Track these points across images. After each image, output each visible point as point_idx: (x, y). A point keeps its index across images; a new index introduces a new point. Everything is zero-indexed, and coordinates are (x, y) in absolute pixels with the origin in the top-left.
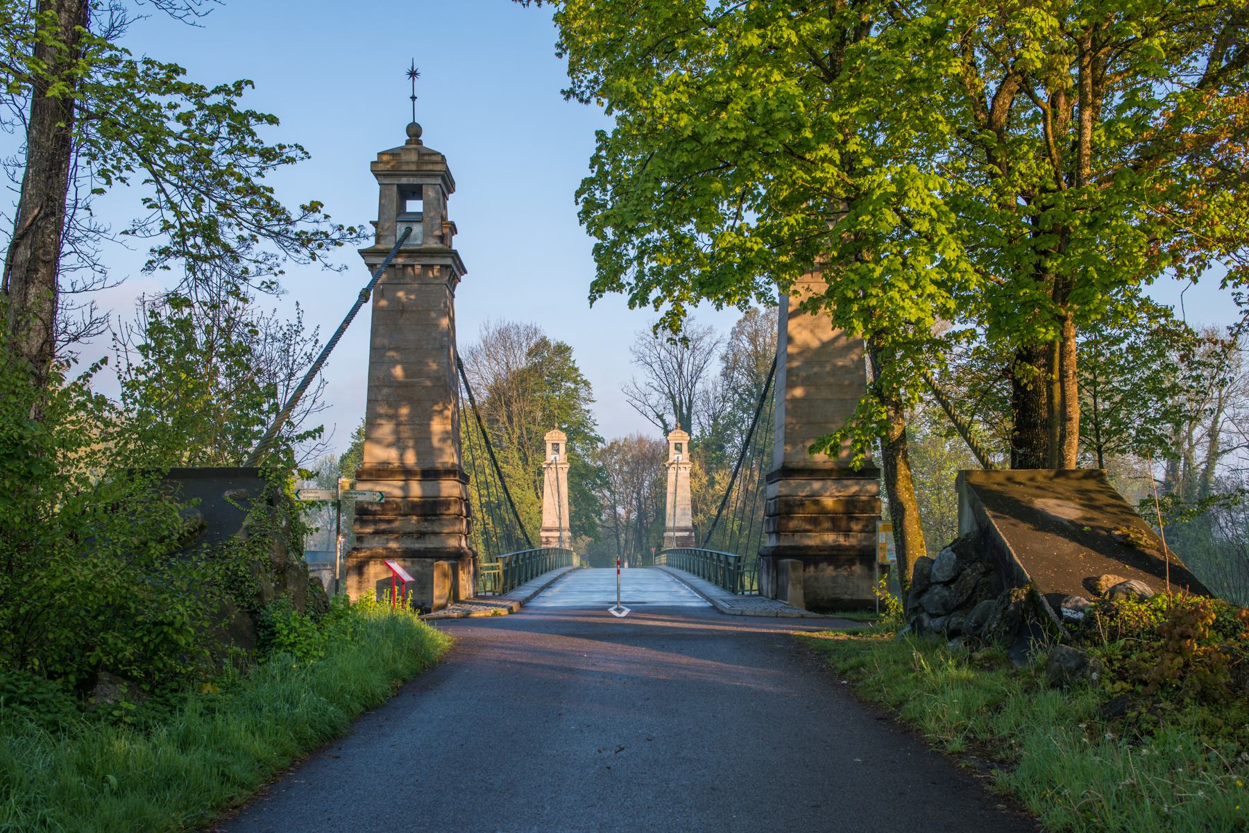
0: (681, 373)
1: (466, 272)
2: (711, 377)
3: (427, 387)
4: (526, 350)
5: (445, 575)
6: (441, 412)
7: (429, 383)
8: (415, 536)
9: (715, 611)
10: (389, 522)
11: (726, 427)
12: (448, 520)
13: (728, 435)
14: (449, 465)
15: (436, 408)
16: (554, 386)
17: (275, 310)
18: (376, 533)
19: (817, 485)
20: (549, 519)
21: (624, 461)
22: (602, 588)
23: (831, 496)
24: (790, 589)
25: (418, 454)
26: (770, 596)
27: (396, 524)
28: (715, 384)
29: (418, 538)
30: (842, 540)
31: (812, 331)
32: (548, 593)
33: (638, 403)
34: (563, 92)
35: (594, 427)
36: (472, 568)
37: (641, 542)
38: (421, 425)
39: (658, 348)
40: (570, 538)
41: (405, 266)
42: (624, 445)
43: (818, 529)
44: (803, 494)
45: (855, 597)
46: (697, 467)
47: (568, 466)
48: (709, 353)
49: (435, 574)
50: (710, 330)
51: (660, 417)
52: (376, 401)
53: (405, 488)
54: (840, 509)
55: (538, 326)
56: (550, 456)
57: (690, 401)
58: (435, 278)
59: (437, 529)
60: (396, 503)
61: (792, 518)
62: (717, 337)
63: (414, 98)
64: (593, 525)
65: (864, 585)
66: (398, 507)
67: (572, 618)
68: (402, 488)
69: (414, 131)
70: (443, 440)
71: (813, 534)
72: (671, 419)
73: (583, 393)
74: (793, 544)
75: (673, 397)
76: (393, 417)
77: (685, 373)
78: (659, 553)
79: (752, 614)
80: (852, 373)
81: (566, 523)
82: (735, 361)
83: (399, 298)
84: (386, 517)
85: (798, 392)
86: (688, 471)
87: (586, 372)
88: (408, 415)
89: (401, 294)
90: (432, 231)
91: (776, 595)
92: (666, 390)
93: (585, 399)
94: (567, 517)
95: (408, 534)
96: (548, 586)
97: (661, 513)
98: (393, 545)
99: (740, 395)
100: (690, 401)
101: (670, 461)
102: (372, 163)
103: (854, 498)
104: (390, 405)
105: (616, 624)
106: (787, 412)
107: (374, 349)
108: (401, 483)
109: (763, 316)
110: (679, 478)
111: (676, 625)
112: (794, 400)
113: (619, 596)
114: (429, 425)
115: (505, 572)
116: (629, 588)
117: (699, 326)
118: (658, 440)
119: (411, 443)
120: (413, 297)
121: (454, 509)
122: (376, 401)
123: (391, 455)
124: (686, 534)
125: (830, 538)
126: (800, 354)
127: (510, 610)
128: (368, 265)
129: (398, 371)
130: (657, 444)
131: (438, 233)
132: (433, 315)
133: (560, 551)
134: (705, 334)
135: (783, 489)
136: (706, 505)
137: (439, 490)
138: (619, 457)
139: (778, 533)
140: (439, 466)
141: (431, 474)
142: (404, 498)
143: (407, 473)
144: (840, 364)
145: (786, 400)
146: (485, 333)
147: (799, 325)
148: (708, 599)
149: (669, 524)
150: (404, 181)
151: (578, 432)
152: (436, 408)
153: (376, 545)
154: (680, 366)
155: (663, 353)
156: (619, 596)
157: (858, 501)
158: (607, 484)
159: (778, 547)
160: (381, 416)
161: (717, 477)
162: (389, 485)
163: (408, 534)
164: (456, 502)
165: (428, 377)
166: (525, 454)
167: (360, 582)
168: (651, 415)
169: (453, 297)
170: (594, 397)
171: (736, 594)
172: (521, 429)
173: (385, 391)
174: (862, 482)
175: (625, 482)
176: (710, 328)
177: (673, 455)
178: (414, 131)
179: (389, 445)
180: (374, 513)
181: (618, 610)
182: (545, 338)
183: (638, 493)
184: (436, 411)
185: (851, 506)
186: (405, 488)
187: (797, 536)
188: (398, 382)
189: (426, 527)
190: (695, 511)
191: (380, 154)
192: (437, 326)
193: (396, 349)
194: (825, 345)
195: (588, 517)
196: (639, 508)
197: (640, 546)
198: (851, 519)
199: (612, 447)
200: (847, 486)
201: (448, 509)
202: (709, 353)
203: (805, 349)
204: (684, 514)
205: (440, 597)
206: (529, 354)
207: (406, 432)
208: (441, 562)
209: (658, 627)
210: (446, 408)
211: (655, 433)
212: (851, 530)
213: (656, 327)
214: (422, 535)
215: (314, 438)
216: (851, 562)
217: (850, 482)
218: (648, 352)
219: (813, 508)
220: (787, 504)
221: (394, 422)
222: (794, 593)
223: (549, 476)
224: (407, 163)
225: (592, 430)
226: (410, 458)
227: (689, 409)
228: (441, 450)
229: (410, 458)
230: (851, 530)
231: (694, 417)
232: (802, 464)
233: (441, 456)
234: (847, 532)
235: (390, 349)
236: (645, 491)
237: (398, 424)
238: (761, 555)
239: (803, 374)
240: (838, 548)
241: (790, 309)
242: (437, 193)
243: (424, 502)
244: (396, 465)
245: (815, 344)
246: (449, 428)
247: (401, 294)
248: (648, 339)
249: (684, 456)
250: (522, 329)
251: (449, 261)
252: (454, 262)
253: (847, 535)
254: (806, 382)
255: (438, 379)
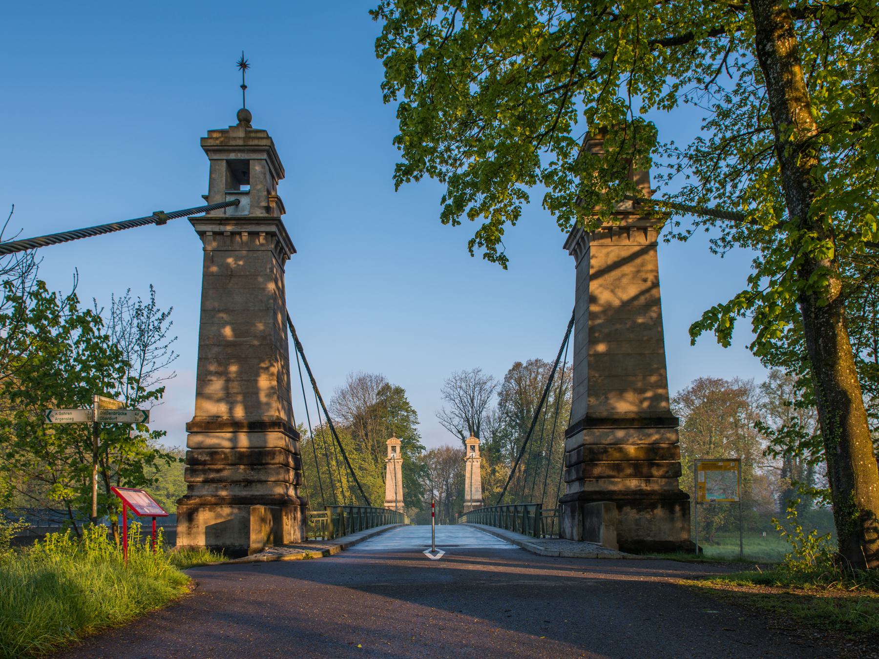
0: (473, 405)
1: (295, 252)
2: (491, 408)
3: (254, 345)
4: (376, 391)
5: (263, 520)
6: (267, 369)
7: (256, 343)
8: (243, 484)
9: (524, 554)
10: (218, 471)
11: (501, 438)
12: (274, 469)
13: (503, 443)
14: (274, 418)
15: (263, 365)
16: (394, 414)
17: (129, 290)
18: (206, 482)
19: (620, 434)
20: (390, 495)
21: (438, 462)
22: (421, 535)
23: (633, 444)
24: (603, 530)
25: (246, 408)
26: (576, 538)
27: (225, 473)
28: (494, 412)
29: (245, 486)
30: (644, 486)
31: (612, 291)
32: (376, 539)
33: (447, 424)
34: (371, 12)
35: (419, 439)
36: (299, 515)
37: (448, 511)
38: (248, 381)
39: (459, 389)
40: (403, 507)
41: (233, 234)
42: (438, 453)
43: (621, 474)
44: (606, 442)
45: (657, 539)
46: (484, 462)
47: (402, 461)
48: (490, 392)
49: (252, 518)
50: (491, 378)
51: (460, 432)
52: (207, 359)
53: (234, 440)
54: (641, 455)
55: (383, 376)
56: (390, 454)
57: (479, 422)
58: (262, 245)
59: (263, 478)
60: (225, 453)
61: (596, 465)
62: (495, 382)
63: (244, 87)
64: (419, 501)
65: (666, 527)
66: (226, 458)
67: (382, 561)
68: (230, 440)
69: (244, 117)
70: (269, 395)
71: (616, 480)
72: (466, 433)
73: (412, 418)
74: (597, 489)
75: (468, 421)
76: (223, 374)
77: (475, 405)
78: (461, 515)
79: (571, 555)
80: (650, 329)
81: (400, 497)
82: (507, 395)
83: (228, 264)
84: (215, 467)
85: (601, 348)
86: (479, 463)
87: (414, 405)
88: (236, 372)
89: (230, 260)
90: (259, 203)
91: (582, 537)
92: (464, 415)
93: (413, 422)
94: (402, 493)
95: (235, 483)
96: (379, 534)
97: (461, 493)
98: (223, 493)
99: (510, 417)
100: (479, 422)
101: (467, 457)
102: (203, 139)
103: (655, 446)
104: (220, 364)
105: (429, 570)
106: (590, 366)
107: (204, 310)
108: (229, 435)
109: (525, 368)
110: (474, 467)
111: (492, 568)
112: (597, 355)
113: (433, 541)
114: (256, 381)
115: (333, 520)
116: (443, 535)
117: (483, 376)
118: (458, 448)
119: (240, 398)
120: (241, 263)
121: (280, 459)
122: (207, 359)
123: (221, 409)
124: (478, 504)
125: (633, 484)
126: (604, 312)
127: (326, 553)
128: (197, 232)
129: (228, 331)
130: (458, 451)
131: (264, 204)
132: (260, 279)
133: (395, 513)
134: (488, 380)
135: (587, 438)
136: (490, 485)
137: (265, 442)
138: (435, 460)
139: (581, 480)
140: (266, 419)
141: (257, 426)
142: (232, 448)
143: (236, 426)
144: (640, 320)
145: (590, 355)
146: (350, 380)
147: (601, 286)
148: (518, 543)
149: (468, 497)
150: (232, 156)
151: (409, 443)
152: (263, 365)
153: (206, 491)
154: (472, 401)
155: (462, 393)
156: (433, 541)
157: (659, 448)
158: (428, 476)
159: (583, 492)
160: (211, 373)
161: (497, 468)
162: (218, 437)
163: (235, 483)
164: (280, 452)
165: (255, 337)
166: (376, 456)
167: (189, 528)
168: (454, 430)
169: (283, 272)
170: (419, 420)
171: (538, 537)
172: (373, 441)
173: (215, 350)
174: (662, 431)
175: (438, 474)
176: (491, 377)
177: (469, 454)
178: (244, 117)
179: (219, 400)
180: (204, 463)
181: (434, 552)
182: (388, 384)
183: (447, 482)
184: (262, 368)
185: (653, 454)
186: (234, 440)
187: (601, 482)
188: (227, 341)
189: (254, 475)
190: (483, 490)
191: (210, 132)
192: (264, 289)
193: (225, 311)
194: (625, 304)
195: (416, 496)
196: (447, 490)
197: (447, 513)
198: (652, 465)
199: (430, 454)
200: (649, 435)
201: (273, 458)
202: (490, 392)
203: (608, 308)
204: (477, 491)
205: (255, 542)
206: (378, 394)
207: (235, 387)
208: (258, 506)
209: (477, 571)
210: (272, 365)
211: (456, 444)
212: (652, 476)
213: (472, 243)
214: (248, 483)
215: (157, 398)
216: (653, 506)
217: (651, 431)
218: (452, 392)
219: (617, 455)
220: (591, 451)
221: (224, 378)
222: (608, 534)
223: (390, 467)
224: (235, 138)
225: (418, 441)
226: (239, 412)
227: (478, 427)
228: (268, 404)
229: (239, 412)
230: (652, 476)
231: (481, 433)
232: (605, 414)
233: (268, 411)
234: (648, 477)
235: (219, 311)
236: (451, 481)
237: (228, 381)
238: (562, 502)
239: (606, 331)
240: (640, 492)
241: (592, 271)
242: (263, 167)
243: (252, 452)
244: (225, 418)
245: (617, 303)
246: (275, 383)
247: (230, 260)
248: (452, 384)
249: (476, 454)
250: (373, 378)
251: (273, 229)
252: (279, 230)
253: (648, 481)
254: (608, 338)
255: (264, 338)
